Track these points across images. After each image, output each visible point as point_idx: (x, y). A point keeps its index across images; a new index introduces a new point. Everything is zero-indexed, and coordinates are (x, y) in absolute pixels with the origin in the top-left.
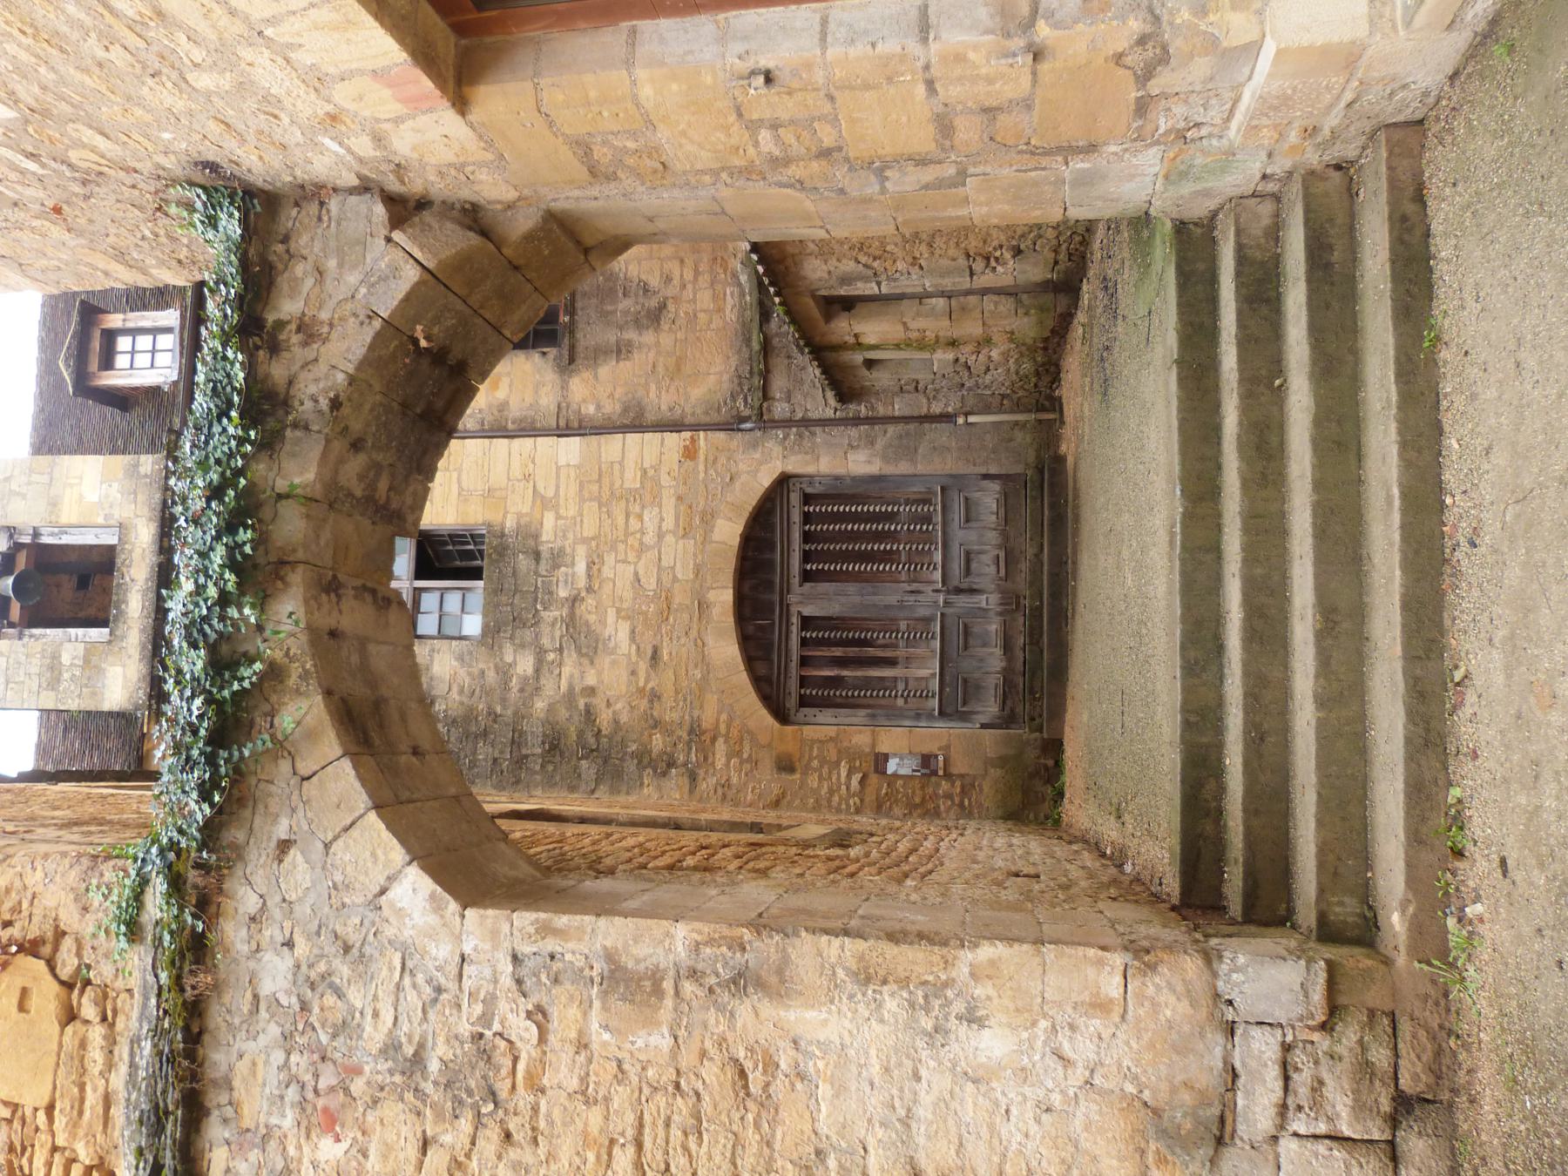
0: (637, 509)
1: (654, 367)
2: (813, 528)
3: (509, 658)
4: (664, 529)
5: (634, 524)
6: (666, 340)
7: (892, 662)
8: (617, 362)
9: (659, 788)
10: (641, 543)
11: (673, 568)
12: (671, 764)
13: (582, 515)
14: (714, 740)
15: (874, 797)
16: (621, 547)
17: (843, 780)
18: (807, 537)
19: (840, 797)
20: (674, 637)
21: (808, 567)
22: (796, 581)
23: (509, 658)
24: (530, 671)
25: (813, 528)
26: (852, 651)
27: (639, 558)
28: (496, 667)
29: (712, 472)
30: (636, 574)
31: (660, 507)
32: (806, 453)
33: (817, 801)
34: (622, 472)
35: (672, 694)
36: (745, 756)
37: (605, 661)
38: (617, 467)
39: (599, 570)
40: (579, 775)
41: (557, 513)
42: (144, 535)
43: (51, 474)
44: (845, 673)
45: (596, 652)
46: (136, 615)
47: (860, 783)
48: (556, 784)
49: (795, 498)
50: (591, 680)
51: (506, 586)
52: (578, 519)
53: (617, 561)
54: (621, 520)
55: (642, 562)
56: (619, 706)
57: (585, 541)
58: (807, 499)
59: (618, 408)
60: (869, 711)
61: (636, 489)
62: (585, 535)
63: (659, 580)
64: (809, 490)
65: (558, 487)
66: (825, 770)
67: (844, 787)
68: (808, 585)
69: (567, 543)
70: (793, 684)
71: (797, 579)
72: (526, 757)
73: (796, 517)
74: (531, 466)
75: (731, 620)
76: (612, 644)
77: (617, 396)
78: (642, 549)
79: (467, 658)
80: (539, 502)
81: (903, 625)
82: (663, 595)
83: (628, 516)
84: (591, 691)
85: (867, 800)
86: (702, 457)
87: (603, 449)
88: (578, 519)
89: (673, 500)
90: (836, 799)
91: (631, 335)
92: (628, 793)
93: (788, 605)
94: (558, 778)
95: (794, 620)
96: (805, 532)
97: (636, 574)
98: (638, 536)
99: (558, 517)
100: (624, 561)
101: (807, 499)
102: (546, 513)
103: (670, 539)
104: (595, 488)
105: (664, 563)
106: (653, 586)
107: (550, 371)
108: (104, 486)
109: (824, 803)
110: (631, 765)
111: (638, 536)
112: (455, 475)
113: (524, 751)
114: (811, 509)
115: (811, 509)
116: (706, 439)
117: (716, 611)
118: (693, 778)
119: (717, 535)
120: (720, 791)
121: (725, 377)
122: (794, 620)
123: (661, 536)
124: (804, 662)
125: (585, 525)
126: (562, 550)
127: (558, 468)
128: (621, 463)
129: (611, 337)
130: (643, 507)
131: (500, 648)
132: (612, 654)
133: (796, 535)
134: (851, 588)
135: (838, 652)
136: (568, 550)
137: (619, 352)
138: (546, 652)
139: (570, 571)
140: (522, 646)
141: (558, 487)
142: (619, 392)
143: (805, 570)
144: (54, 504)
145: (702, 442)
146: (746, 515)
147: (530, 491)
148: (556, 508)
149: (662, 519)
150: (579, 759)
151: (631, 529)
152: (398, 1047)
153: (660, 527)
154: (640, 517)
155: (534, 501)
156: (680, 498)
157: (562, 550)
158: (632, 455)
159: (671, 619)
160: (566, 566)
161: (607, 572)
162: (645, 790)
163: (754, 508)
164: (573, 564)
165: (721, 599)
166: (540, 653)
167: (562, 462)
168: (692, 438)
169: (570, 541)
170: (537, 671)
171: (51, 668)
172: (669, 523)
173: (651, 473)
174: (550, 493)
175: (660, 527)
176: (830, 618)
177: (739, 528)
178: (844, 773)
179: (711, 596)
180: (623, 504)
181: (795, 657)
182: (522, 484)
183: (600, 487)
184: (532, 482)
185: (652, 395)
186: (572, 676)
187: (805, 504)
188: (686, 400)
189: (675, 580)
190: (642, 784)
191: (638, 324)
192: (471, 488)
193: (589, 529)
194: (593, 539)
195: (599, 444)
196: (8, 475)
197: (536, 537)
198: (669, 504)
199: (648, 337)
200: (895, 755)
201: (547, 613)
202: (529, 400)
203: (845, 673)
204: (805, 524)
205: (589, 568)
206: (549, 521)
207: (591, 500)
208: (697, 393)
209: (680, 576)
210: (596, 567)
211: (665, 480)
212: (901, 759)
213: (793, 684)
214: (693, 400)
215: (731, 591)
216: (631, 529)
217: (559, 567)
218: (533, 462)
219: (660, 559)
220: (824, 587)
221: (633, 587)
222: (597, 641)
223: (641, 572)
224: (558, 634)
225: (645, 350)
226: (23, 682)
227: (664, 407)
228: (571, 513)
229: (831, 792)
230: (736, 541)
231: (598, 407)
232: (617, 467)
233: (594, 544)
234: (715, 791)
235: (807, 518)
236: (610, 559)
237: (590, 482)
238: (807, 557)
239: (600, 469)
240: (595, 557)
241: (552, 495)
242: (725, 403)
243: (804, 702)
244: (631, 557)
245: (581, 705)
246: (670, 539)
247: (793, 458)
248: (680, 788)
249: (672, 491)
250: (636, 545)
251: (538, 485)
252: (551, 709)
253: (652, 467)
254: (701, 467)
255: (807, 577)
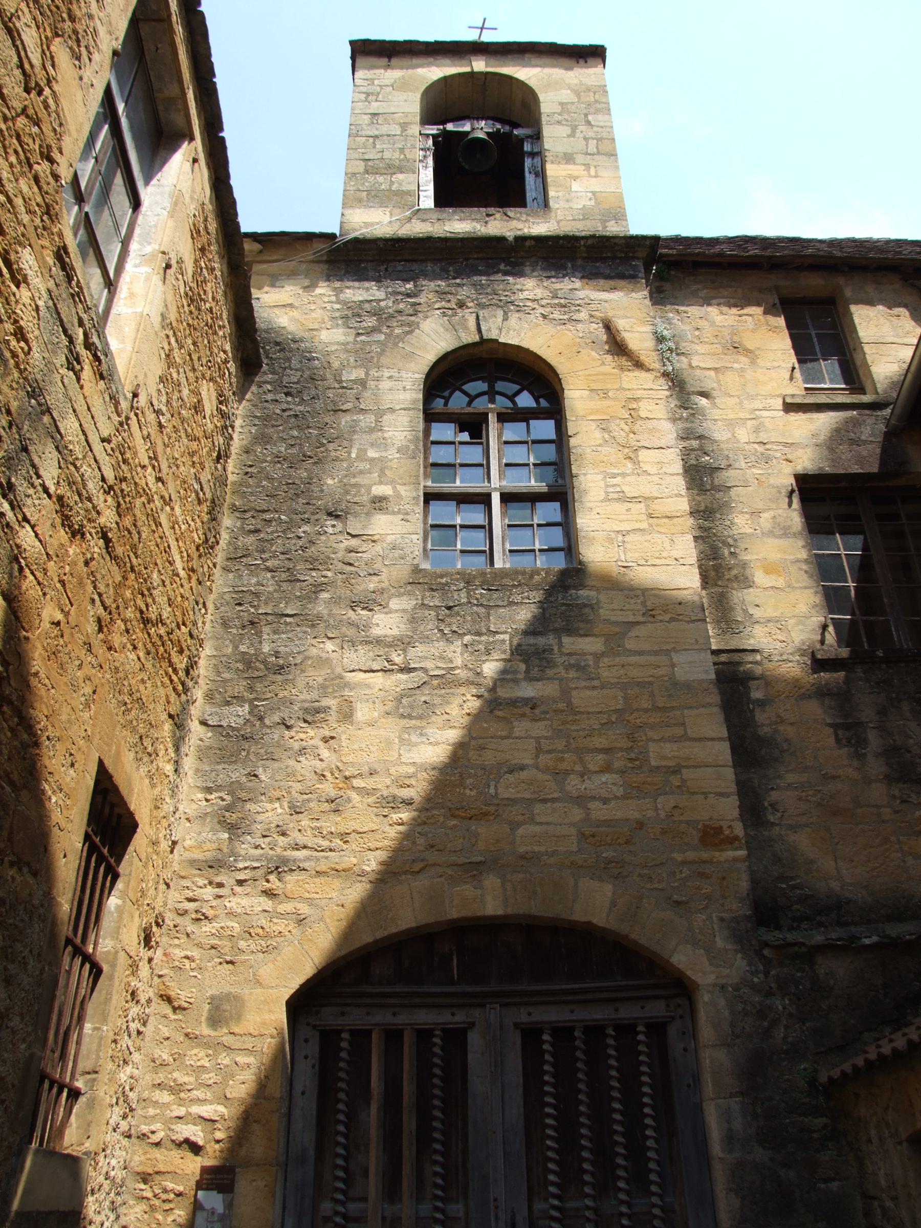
0: (618, 764)
1: (834, 777)
2: (611, 1041)
3: (395, 604)
4: (590, 805)
5: (595, 761)
6: (878, 793)
7: (392, 1192)
8: (830, 725)
9: (203, 817)
10: (567, 773)
11: (532, 821)
12: (234, 829)
13: (603, 687)
14: (269, 894)
15: (161, 1167)
16: (560, 744)
17: (196, 1109)
18: (594, 1032)
19: (166, 1106)
20: (426, 828)
21: (546, 1037)
22: (523, 1016)
23: (395, 604)
24: (376, 632)
25: (611, 1041)
26: (409, 1122)
27: (546, 770)
28: (382, 591)
29: (686, 872)
30: (522, 768)
31: (625, 797)
32: (733, 1025)
33: (164, 1065)
34: (674, 740)
35: (342, 829)
36: (242, 944)
37: (391, 729)
38: (679, 731)
39: (523, 715)
40: (228, 703)
41: (603, 654)
42: (539, 227)
43: (598, 153)
44: (374, 1107)
45: (403, 716)
46: (447, 228)
47: (187, 1141)
48: (219, 673)
49: (657, 1009)
50: (362, 713)
51: (496, 595)
52: (596, 683)
53: (538, 740)
54: (599, 742)
55: (541, 776)
56: (325, 753)
57: (566, 693)
58: (657, 1029)
59: (765, 731)
60: (312, 1153)
61: (647, 760)
62: (574, 693)
63: (513, 801)
64: (672, 1031)
65: (640, 653)
66: (210, 1077)
67: (182, 1111)
68: (517, 1039)
69: (561, 670)
70: (356, 1018)
71: (524, 1018)
72: (259, 634)
73: (628, 1012)
74: (667, 617)
75: (453, 913)
76: (414, 738)
77: (781, 728)
78: (560, 775)
79: (397, 553)
80: (617, 630)
81: (457, 1209)
82: (492, 809)
83: (607, 751)
84: (347, 716)
85: (156, 1153)
86: (705, 855)
87: (701, 710)
88: (596, 683)
89: (636, 815)
90: (165, 1097)
91: (874, 741)
92: (197, 770)
93: (483, 1006)
94: (226, 675)
95: (460, 1017)
96: (602, 1028)
97: (522, 768)
98: (578, 768)
99: (598, 656)
100: (539, 750)
101: (657, 1029)
102: (601, 640)
103: (577, 814)
104: (645, 704)
105: (538, 808)
106: (504, 793)
107: (804, 636)
108: (590, 195)
109: (161, 1077)
110: (237, 774)
111: (578, 768)
112: (644, 525)
113: (266, 629)
114: (641, 1037)
115: (641, 1037)
116: (735, 860)
117: (467, 890)
118: (214, 865)
119: (586, 884)
120: (191, 906)
121: (835, 886)
122: (460, 1017)
123: (581, 800)
124: (393, 1036)
125: (588, 693)
126: (551, 664)
127: (667, 652)
128: (685, 738)
129: (867, 713)
130: (622, 772)
131: (409, 593)
132: (402, 740)
133: (598, 1014)
134: (515, 1110)
135: (408, 1088)
136: (550, 673)
137: (847, 727)
138: (404, 650)
139: (520, 676)
140: (413, 620)
141: (640, 653)
142: (790, 731)
143: (541, 1032)
144: (568, 158)
145: (730, 854)
146: (624, 929)
147: (631, 618)
148: (610, 652)
149: (605, 801)
150: (251, 702)
151: (587, 758)
152: (347, 492)
153: (593, 798)
154: (607, 769)
155: (616, 623)
156: (640, 825)
157: (551, 664)
158: (698, 752)
159: (454, 822)
160: (527, 671)
161: (521, 727)
162: (200, 796)
163: (636, 943)
164: (530, 679)
165: (489, 899)
166: (403, 643)
167: (677, 658)
168: (736, 838)
169: (563, 673)
170: (378, 642)
171: (389, 167)
172: (599, 811)
173: (675, 781)
174: (630, 644)
175: (593, 798)
176: (465, 1080)
177: (600, 919)
178: (206, 1110)
179: (491, 882)
180: (624, 743)
181: (404, 1018)
182: (639, 607)
183: (646, 711)
184: (643, 619)
185: (791, 778)
186: (368, 686)
187: (648, 1026)
188: (792, 827)
189: (515, 826)
190: (209, 790)
191: (891, 752)
192: (628, 546)
193: (583, 698)
194: (569, 704)
195: (710, 705)
196: (593, 123)
197: (570, 631)
198: (631, 811)
199: (876, 767)
200: (229, 1205)
201: (459, 650)
202: (757, 613)
203: (374, 1107)
204: (617, 1028)
205: (526, 701)
206: (590, 645)
207: (626, 698)
208: (803, 842)
209: (521, 831)
210: (527, 710)
211: (665, 803)
212: (222, 1218)
213: (356, 1018)
214: (792, 837)
215: (500, 912)
216: (587, 758)
217: (526, 661)
218: (672, 620)
219: (544, 801)
220: (514, 1061)
221: (500, 765)
222: (420, 717)
223: (524, 775)
224: (429, 665)
225: (855, 763)
226: (374, 147)
227: (774, 796)
228: (605, 673)
229: (176, 1089)
230: (579, 915)
231: (762, 703)
232: (679, 731)
233: (561, 706)
234: (190, 900)
235: (626, 1030)
236: (540, 729)
237: (652, 695)
238: (562, 1033)
239: (673, 708)
240: (543, 708)
241: (628, 646)
242: (794, 887)
243: (328, 1038)
244: (544, 759)
245: (325, 702)
246: (577, 814)
247: (722, 1002)
248: (200, 845)
249: (650, 813)
250: (564, 766)
251: (642, 627)
252: (323, 662)
253: (684, 781)
254: (690, 855)
255: (531, 1034)
